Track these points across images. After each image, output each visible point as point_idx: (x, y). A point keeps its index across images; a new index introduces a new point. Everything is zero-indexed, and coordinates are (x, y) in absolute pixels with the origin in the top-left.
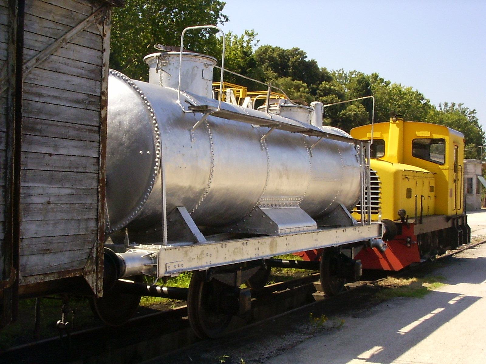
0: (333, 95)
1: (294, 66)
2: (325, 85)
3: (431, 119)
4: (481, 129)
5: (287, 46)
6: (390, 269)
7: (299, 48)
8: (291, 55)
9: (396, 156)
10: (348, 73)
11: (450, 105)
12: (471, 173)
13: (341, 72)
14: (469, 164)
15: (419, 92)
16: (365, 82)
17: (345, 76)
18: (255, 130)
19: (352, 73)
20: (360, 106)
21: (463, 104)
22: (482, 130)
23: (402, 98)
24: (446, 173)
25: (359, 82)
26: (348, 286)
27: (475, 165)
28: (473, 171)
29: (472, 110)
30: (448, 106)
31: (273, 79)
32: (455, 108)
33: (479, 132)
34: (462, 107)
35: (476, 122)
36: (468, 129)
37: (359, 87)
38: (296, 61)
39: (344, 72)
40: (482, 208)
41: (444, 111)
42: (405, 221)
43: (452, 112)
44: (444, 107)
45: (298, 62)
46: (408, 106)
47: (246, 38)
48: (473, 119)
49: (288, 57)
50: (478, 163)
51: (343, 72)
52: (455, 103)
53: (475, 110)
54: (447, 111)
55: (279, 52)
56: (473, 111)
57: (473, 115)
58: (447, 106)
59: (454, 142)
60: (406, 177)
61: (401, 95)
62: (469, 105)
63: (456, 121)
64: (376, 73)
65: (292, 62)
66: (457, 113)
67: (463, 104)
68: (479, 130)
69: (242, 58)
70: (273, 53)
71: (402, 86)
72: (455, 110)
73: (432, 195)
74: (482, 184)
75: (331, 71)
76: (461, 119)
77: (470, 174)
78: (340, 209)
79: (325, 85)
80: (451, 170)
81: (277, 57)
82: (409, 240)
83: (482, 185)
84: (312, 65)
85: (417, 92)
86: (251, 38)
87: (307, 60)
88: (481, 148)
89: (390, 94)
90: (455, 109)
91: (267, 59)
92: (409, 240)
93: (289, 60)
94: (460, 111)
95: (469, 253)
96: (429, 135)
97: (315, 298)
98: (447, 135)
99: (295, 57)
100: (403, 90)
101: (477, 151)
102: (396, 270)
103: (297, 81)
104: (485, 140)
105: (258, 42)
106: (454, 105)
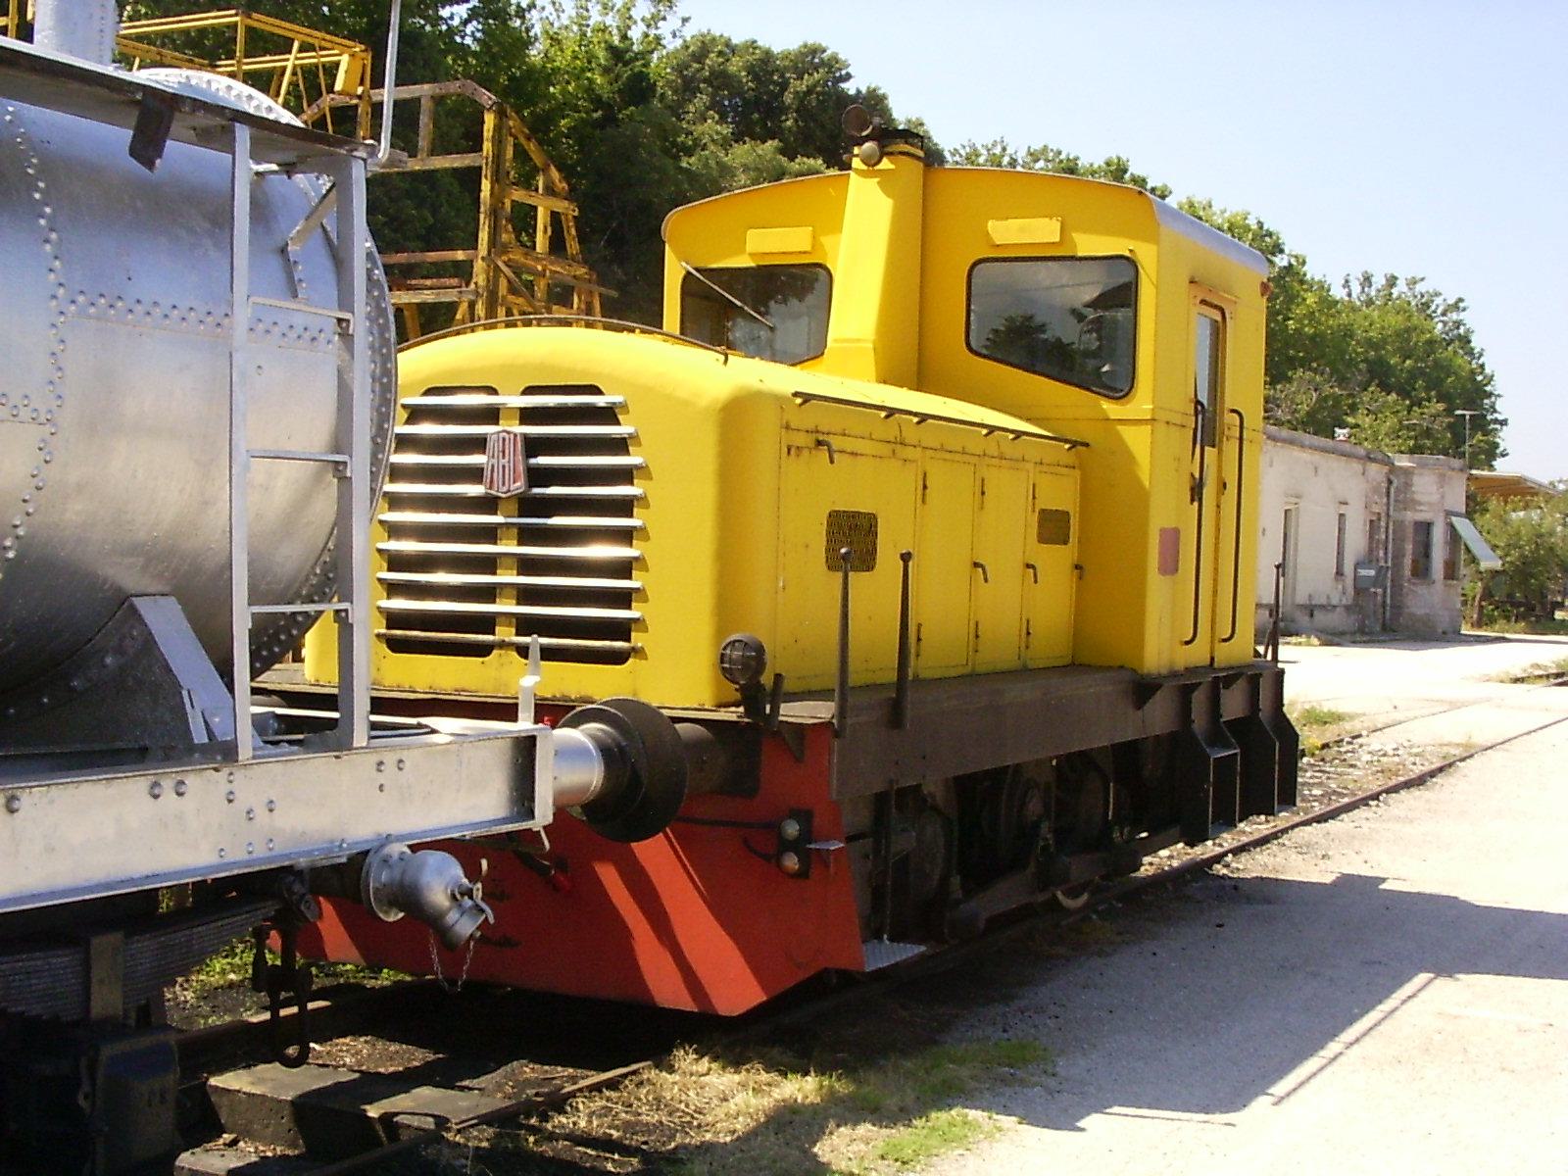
1: (802, 110)
4: (1482, 366)
5: (781, 39)
6: (688, 1005)
7: (824, 45)
8: (795, 69)
9: (871, 346)
10: (1021, 156)
11: (1379, 281)
12: (1430, 504)
13: (998, 151)
14: (1421, 474)
15: (1265, 227)
17: (1013, 163)
19: (1034, 156)
21: (1423, 279)
22: (1486, 367)
24: (1138, 441)
26: (387, 1119)
27: (1442, 476)
28: (1435, 498)
29: (1451, 301)
30: (1373, 288)
31: (712, 147)
32: (1395, 292)
33: (1473, 372)
34: (1420, 288)
35: (1465, 340)
36: (1435, 361)
38: (810, 91)
39: (1008, 152)
40: (1466, 630)
41: (1358, 303)
44: (1359, 289)
48: (1455, 332)
49: (782, 76)
50: (1453, 469)
51: (1004, 149)
52: (1396, 274)
53: (1461, 300)
56: (1457, 303)
57: (1454, 316)
58: (1370, 286)
59: (1191, 282)
60: (819, 443)
62: (1443, 283)
63: (1398, 334)
64: (1119, 159)
66: (1403, 310)
67: (1423, 279)
68: (1474, 366)
69: (606, 71)
72: (1397, 299)
73: (1056, 560)
74: (1466, 545)
75: (964, 147)
77: (1422, 508)
80: (1174, 432)
81: (743, 74)
82: (792, 829)
83: (1468, 550)
85: (1261, 225)
86: (662, 8)
87: (850, 87)
88: (1464, 416)
90: (1394, 296)
91: (705, 81)
93: (784, 86)
94: (1413, 303)
95: (1301, 849)
96: (1057, 239)
98: (1153, 238)
99: (806, 76)
101: (1450, 426)
102: (720, 1013)
103: (805, 159)
104: (1494, 403)
105: (683, 25)
106: (1392, 281)
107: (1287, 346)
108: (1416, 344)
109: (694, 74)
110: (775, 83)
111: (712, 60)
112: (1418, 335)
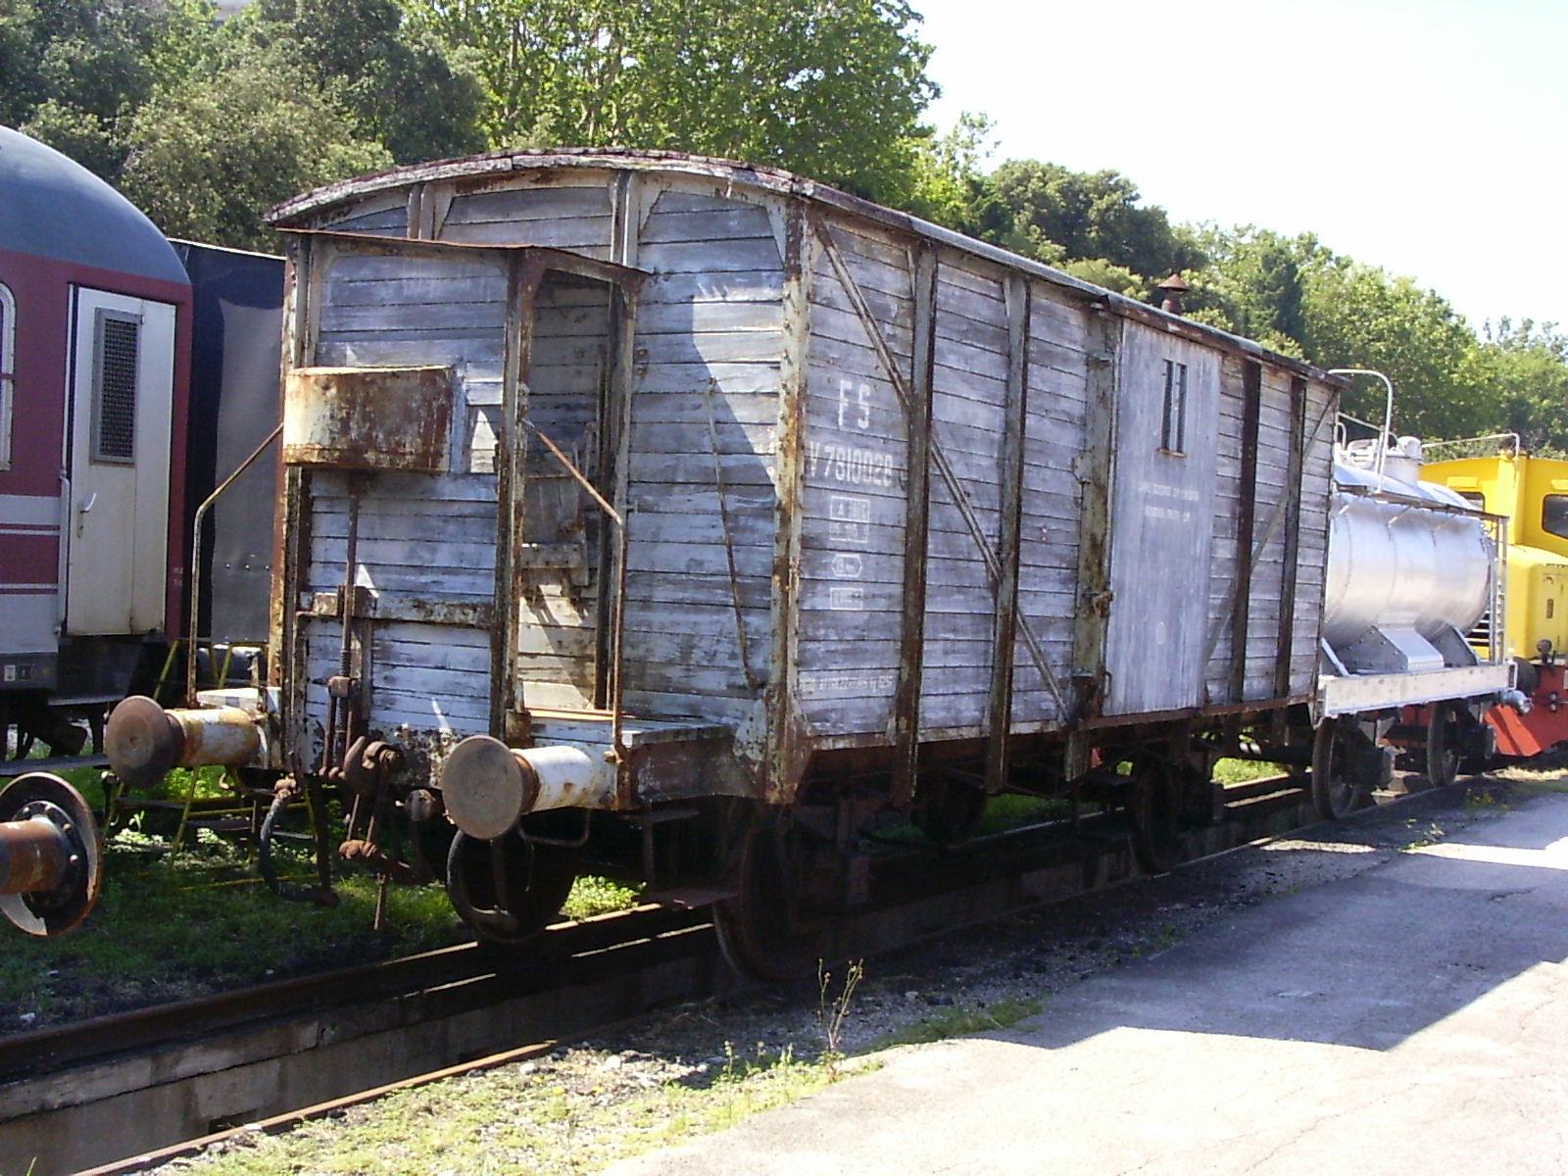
0: (1212, 309)
1: (1103, 224)
2: (1188, 277)
3: (1468, 375)
5: (1083, 161)
6: (1514, 753)
11: (1516, 325)
16: (1286, 262)
18: (1378, 508)
19: (1241, 233)
20: (1286, 344)
23: (1387, 310)
25: (1269, 263)
32: (1531, 335)
34: (1554, 332)
37: (1269, 278)
38: (1108, 209)
39: (1220, 230)
42: (1550, 661)
43: (1524, 347)
45: (1116, 211)
46: (1404, 335)
47: (965, 134)
49: (1086, 196)
51: (1217, 228)
54: (1509, 344)
55: (1061, 181)
58: (1509, 329)
61: (1384, 302)
65: (1098, 210)
66: (1537, 354)
70: (1046, 184)
71: (1386, 272)
76: (1552, 372)
78: (1452, 634)
79: (1191, 280)
84: (1152, 221)
85: (1433, 292)
87: (1138, 206)
89: (1351, 296)
90: (1530, 338)
92: (1554, 697)
93: (1089, 204)
97: (1377, 801)
99: (1106, 197)
100: (1392, 288)
102: (1526, 754)
103: (1115, 268)
106: (1528, 325)
107: (1451, 395)
108: (1553, 385)
109: (1018, 195)
110: (1081, 202)
111: (1034, 184)
112: (1555, 378)
